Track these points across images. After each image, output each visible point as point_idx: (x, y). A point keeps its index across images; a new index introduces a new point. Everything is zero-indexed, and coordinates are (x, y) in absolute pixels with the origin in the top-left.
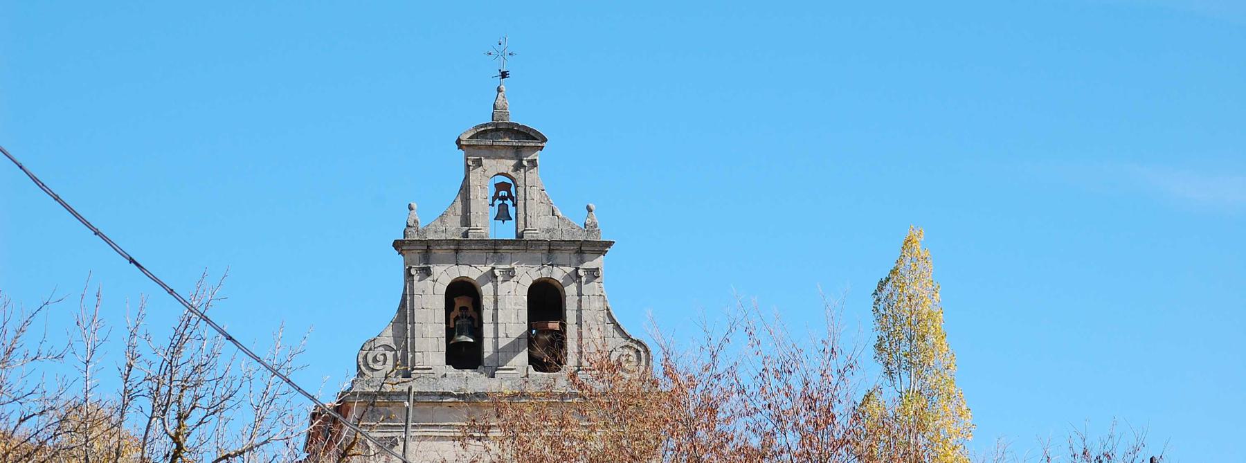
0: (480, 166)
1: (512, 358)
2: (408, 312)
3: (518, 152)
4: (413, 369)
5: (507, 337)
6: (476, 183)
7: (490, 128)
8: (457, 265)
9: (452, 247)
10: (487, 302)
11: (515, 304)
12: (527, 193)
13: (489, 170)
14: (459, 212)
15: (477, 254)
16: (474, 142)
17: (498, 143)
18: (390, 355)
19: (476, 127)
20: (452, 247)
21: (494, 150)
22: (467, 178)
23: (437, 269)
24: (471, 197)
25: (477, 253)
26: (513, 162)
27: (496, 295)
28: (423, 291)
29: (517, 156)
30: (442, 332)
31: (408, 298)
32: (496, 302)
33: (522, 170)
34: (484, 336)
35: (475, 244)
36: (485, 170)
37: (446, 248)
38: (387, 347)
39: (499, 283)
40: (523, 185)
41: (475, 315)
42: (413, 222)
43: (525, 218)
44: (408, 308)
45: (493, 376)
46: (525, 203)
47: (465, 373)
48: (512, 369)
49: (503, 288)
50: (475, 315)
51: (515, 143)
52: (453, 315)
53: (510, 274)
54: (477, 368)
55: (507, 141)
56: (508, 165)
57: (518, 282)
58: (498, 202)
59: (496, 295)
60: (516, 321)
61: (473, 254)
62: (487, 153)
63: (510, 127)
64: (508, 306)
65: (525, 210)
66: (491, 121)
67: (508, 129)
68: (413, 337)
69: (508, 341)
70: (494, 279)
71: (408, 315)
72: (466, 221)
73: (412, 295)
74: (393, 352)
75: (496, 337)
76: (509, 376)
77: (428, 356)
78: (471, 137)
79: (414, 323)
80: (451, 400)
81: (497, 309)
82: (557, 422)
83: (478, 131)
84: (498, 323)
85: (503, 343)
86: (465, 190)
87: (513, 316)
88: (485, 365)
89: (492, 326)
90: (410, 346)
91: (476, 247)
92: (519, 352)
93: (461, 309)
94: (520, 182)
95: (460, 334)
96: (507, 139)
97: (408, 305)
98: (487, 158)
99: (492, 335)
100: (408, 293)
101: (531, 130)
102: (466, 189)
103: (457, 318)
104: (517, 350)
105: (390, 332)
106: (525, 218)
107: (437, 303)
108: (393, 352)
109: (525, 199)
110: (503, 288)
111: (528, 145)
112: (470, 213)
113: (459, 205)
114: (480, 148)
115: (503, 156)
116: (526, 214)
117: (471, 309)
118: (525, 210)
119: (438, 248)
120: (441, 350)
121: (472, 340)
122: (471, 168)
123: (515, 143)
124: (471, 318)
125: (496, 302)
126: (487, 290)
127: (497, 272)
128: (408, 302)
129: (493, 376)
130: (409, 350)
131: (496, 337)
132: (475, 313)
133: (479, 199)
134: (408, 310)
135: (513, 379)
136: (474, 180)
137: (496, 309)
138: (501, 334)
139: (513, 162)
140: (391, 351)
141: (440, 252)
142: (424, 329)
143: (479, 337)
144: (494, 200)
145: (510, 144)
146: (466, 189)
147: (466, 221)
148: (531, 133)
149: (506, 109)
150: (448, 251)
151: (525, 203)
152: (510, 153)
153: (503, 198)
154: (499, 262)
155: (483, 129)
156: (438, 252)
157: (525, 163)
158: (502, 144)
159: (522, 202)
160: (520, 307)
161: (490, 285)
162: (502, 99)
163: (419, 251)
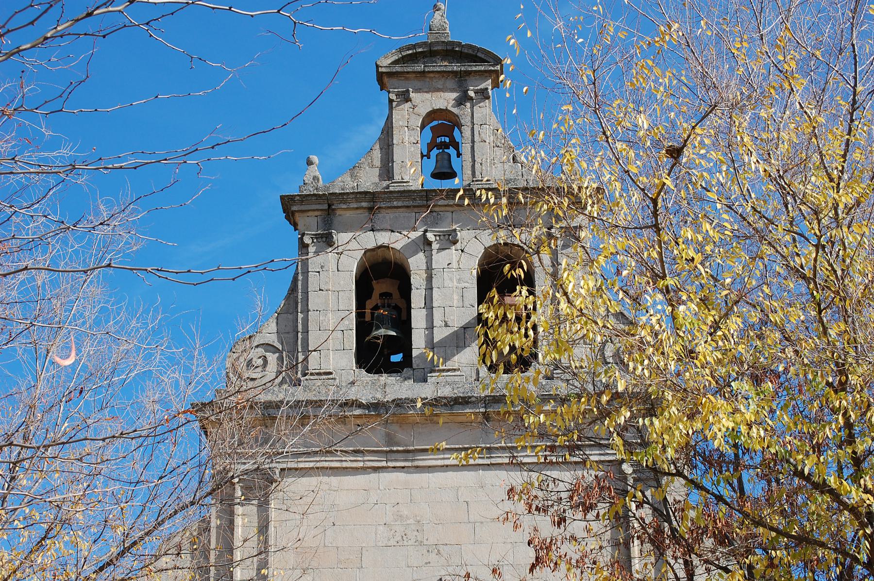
0: (407, 102)
1: (454, 355)
2: (300, 297)
3: (461, 79)
4: (305, 375)
5: (446, 325)
6: (401, 123)
7: (420, 50)
8: (373, 230)
9: (364, 204)
10: (417, 280)
11: (459, 281)
12: (476, 133)
13: (420, 106)
14: (377, 162)
15: (402, 215)
16: (398, 68)
17: (431, 69)
18: (272, 358)
19: (401, 50)
20: (364, 204)
21: (428, 80)
22: (390, 118)
23: (341, 238)
24: (395, 142)
25: (402, 214)
26: (455, 95)
27: (429, 269)
28: (322, 267)
29: (460, 86)
30: (351, 322)
31: (300, 277)
32: (429, 279)
33: (468, 105)
34: (413, 326)
35: (397, 199)
36: (414, 107)
37: (356, 206)
38: (269, 347)
39: (434, 252)
40: (469, 124)
41: (402, 304)
42: (312, 180)
43: (473, 166)
44: (300, 291)
45: (425, 381)
46: (473, 148)
47: (383, 378)
48: (455, 370)
49: (440, 259)
50: (402, 304)
51: (456, 67)
52: (370, 304)
53: (450, 239)
54: (402, 298)
55: (443, 65)
56: (445, 100)
57: (462, 251)
58: (435, 152)
59: (429, 269)
60: (461, 304)
61: (397, 215)
62: (418, 84)
63: (449, 48)
64: (447, 283)
65: (473, 156)
66: (420, 188)
67: (447, 50)
68: (306, 331)
69: (447, 332)
70: (427, 248)
71: (299, 301)
72: (387, 171)
73: (306, 272)
74: (277, 355)
75: (430, 327)
76: (449, 379)
77: (327, 356)
78: (395, 62)
79: (308, 311)
80: (358, 412)
81: (432, 289)
82: (712, 131)
83: (404, 54)
84: (432, 308)
85: (440, 334)
86: (388, 132)
87: (456, 297)
88: (414, 366)
89: (424, 312)
90: (302, 344)
91: (400, 204)
92: (465, 347)
93: (382, 295)
94: (465, 120)
95: (378, 328)
96: (446, 64)
97: (300, 287)
98: (417, 90)
99: (423, 324)
100: (300, 272)
101: (479, 49)
102: (388, 132)
103: (376, 308)
104: (462, 344)
105: (272, 326)
106: (473, 166)
107: (342, 282)
108: (277, 355)
109: (473, 142)
110: (440, 259)
111: (474, 69)
112: (393, 162)
113: (377, 154)
114: (407, 79)
115: (441, 87)
116: (474, 161)
117: (396, 295)
118: (473, 156)
119: (344, 206)
120: (347, 347)
121: (395, 334)
122: (394, 104)
123: (456, 67)
124: (396, 308)
125: (429, 279)
126: (416, 264)
127: (430, 236)
128: (300, 283)
129: (425, 381)
130: (300, 350)
131: (430, 327)
132: (403, 301)
133: (406, 144)
134: (300, 294)
135: (455, 383)
136: (399, 120)
137: (430, 289)
138: (438, 322)
139: (455, 95)
140: (274, 353)
141: (348, 214)
142: (321, 318)
143: (404, 325)
144: (430, 150)
145: (449, 69)
146: (388, 132)
147: (387, 171)
148: (479, 54)
149: (445, 30)
150: (359, 212)
151: (473, 148)
152: (451, 83)
153: (445, 146)
154: (435, 224)
155: (410, 52)
156: (344, 214)
157: (471, 94)
158: (438, 69)
159: (469, 146)
160: (466, 285)
161: (421, 256)
162: (440, 18)
163: (317, 213)
